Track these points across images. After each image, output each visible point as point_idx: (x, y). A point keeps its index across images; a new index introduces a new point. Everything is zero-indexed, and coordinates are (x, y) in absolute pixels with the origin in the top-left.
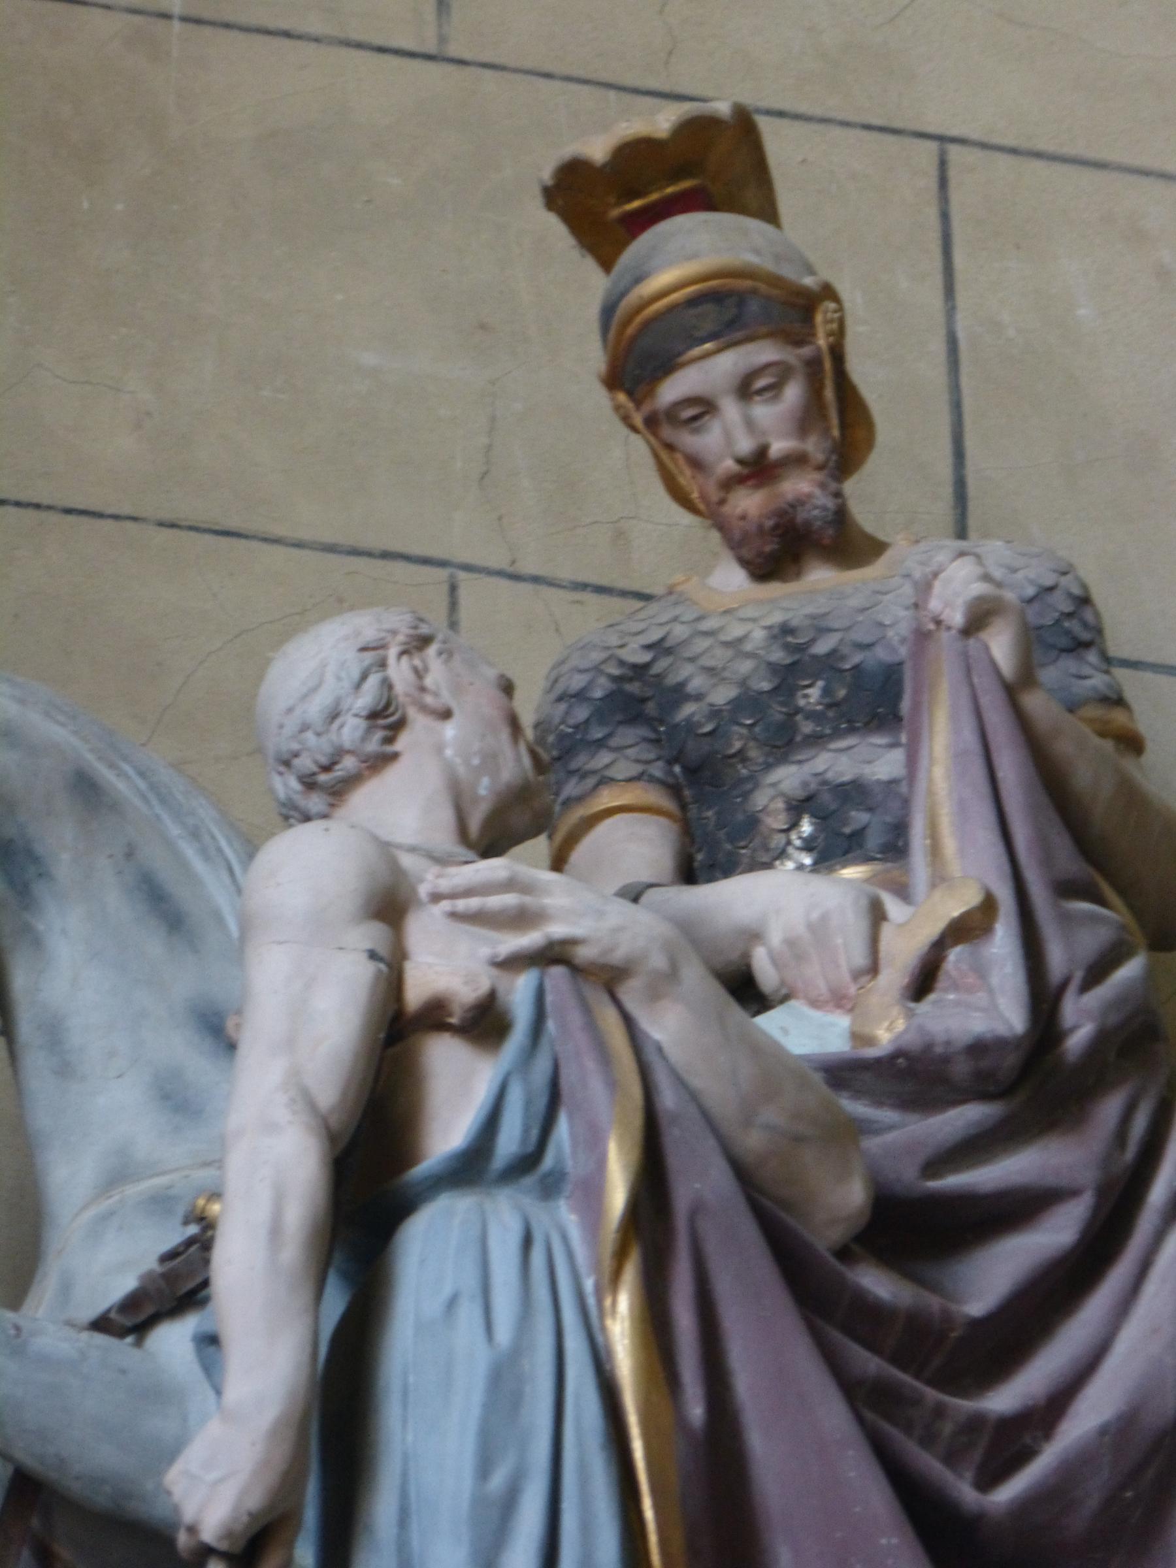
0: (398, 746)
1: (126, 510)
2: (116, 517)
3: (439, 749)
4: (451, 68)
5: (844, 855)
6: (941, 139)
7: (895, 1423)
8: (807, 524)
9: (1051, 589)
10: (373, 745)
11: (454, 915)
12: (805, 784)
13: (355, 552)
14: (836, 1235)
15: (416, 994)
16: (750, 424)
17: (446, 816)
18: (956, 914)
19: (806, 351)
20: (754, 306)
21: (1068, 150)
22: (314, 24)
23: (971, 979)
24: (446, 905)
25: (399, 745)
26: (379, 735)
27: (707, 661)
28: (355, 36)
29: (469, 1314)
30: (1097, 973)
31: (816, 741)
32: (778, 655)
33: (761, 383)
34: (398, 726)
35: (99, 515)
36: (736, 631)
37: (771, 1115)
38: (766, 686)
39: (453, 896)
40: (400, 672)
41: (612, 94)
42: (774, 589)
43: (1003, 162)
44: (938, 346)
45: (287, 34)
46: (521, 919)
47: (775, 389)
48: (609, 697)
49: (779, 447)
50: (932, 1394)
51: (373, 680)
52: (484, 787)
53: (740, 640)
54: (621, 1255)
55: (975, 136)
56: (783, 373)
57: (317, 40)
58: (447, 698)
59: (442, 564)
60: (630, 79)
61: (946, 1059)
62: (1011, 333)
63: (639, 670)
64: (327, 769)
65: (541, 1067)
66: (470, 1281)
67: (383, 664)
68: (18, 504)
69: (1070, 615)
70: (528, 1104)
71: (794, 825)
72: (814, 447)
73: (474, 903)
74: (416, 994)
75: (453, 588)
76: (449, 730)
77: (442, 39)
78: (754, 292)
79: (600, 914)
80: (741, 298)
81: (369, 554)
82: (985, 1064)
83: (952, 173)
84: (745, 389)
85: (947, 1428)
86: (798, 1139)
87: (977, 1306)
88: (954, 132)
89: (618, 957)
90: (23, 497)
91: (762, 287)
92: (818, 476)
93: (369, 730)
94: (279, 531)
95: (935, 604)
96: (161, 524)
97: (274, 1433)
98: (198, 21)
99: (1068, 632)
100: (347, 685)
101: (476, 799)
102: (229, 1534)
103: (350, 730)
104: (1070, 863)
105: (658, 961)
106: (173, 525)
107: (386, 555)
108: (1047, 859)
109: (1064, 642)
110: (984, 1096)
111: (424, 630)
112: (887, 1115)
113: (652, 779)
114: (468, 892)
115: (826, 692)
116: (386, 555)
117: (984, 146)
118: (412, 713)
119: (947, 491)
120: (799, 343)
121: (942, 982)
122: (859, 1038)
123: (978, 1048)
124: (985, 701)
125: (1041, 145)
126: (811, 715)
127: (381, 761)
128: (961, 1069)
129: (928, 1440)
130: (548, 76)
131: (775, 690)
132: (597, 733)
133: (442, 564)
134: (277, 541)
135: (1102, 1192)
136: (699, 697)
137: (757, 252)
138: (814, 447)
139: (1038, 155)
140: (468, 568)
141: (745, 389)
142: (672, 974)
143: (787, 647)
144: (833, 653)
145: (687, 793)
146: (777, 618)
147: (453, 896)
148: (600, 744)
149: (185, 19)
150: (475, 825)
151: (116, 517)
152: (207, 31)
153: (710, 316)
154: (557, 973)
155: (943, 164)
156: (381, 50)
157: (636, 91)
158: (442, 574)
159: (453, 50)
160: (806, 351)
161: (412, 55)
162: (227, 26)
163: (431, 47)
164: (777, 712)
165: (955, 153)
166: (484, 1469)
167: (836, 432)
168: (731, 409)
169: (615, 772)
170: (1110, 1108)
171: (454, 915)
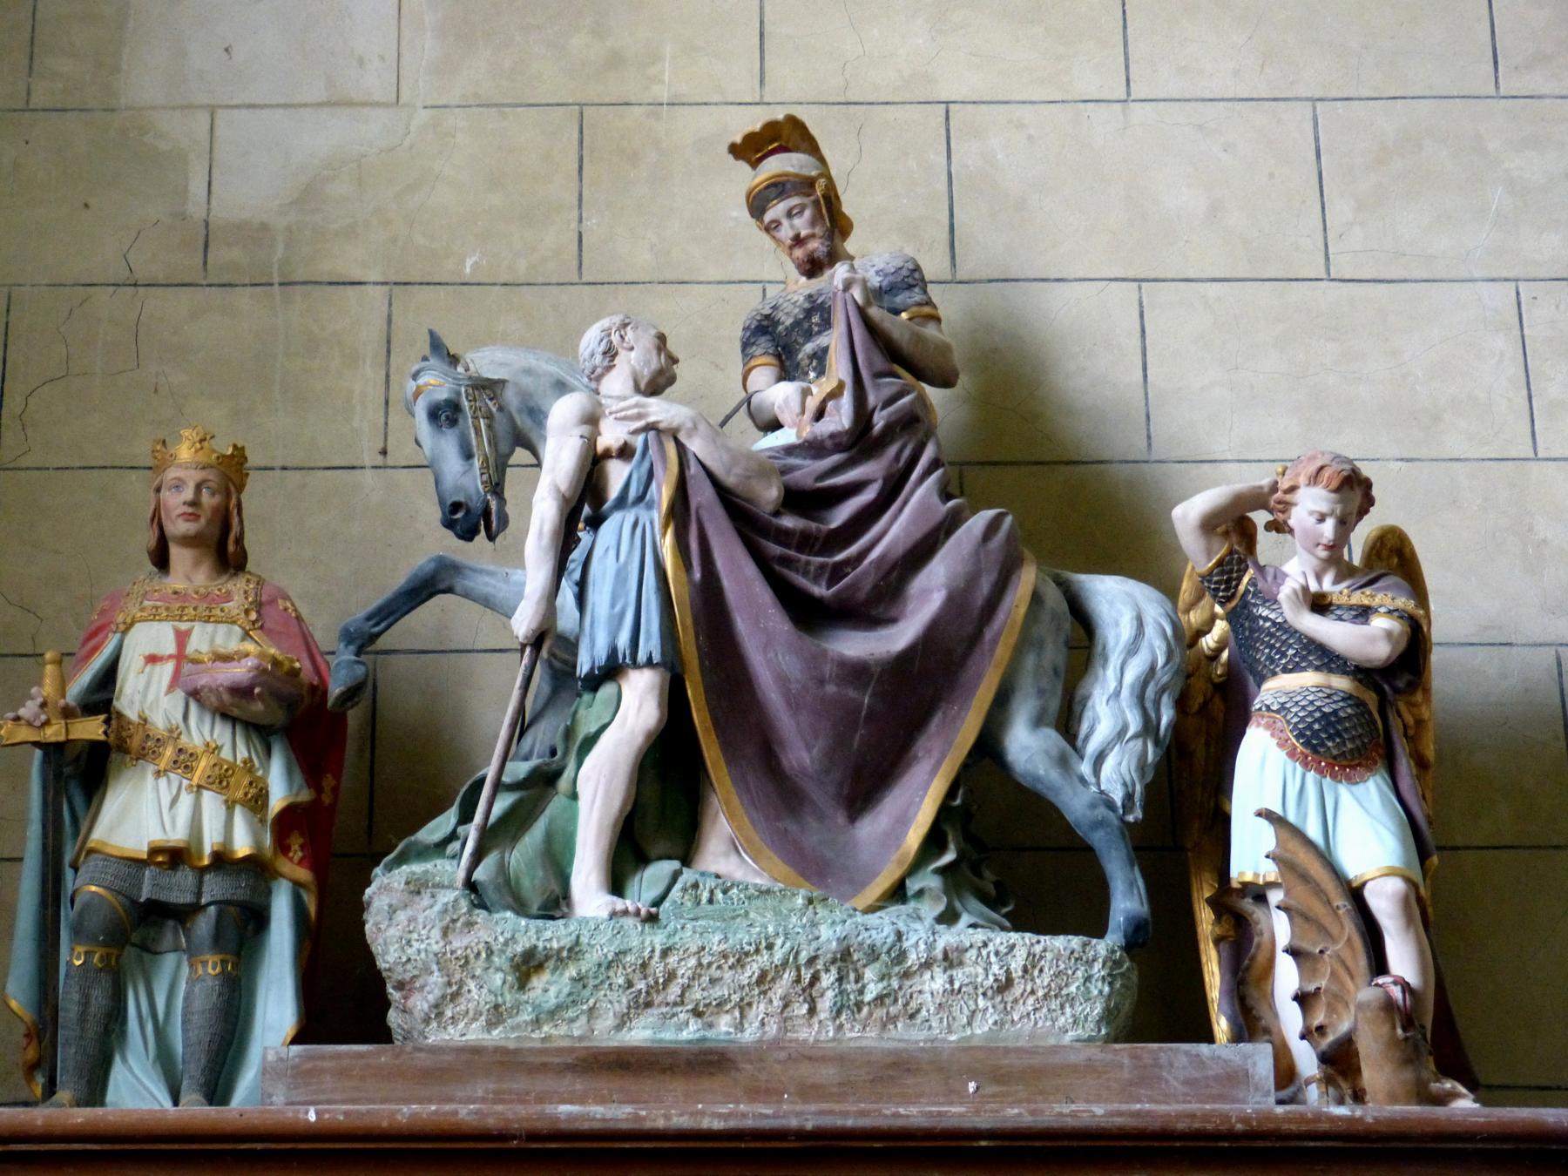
0: (616, 362)
1: (647, 280)
2: (643, 283)
3: (629, 362)
4: (765, 107)
5: (413, 416)
6: (947, 103)
7: (790, 569)
8: (819, 258)
9: (901, 268)
10: (606, 363)
11: (616, 419)
12: (813, 349)
13: (729, 282)
14: (770, 508)
15: (600, 447)
16: (792, 226)
17: (631, 384)
18: (829, 390)
19: (812, 198)
20: (789, 186)
21: (996, 99)
22: (715, 99)
23: (834, 412)
24: (614, 416)
25: (616, 362)
26: (608, 359)
27: (786, 311)
28: (730, 100)
29: (612, 553)
30: (888, 403)
31: (819, 333)
32: (807, 305)
33: (794, 212)
34: (614, 356)
35: (638, 283)
36: (796, 298)
37: (737, 470)
38: (801, 316)
39: (616, 412)
40: (615, 338)
41: (824, 106)
42: (814, 281)
43: (970, 107)
44: (944, 178)
45: (705, 104)
46: (639, 416)
47: (801, 213)
48: (757, 327)
49: (803, 233)
50: (804, 557)
51: (605, 341)
52: (646, 372)
53: (796, 302)
54: (666, 527)
55: (960, 100)
56: (802, 208)
57: (716, 104)
58: (632, 343)
59: (761, 282)
60: (831, 100)
61: (822, 441)
62: (972, 168)
63: (767, 317)
64: (593, 373)
65: (646, 465)
66: (613, 543)
67: (610, 335)
68: (609, 283)
69: (908, 277)
70: (639, 479)
71: (811, 363)
72: (818, 230)
73: (623, 414)
74: (600, 447)
75: (764, 290)
76: (633, 354)
77: (762, 96)
78: (788, 181)
79: (668, 411)
80: (783, 184)
81: (734, 282)
82: (837, 440)
83: (951, 114)
84: (789, 214)
85: (812, 568)
86: (749, 478)
87: (834, 525)
88: (952, 99)
89: (675, 425)
90: (610, 280)
91: (791, 178)
92: (820, 241)
93: (604, 359)
94: (702, 279)
95: (835, 283)
96: (660, 283)
97: (538, 603)
98: (673, 104)
99: (907, 283)
100: (597, 343)
101: (643, 376)
102: (526, 637)
103: (598, 359)
104: (880, 363)
105: (689, 425)
106: (663, 283)
107: (740, 282)
108: (870, 364)
109: (905, 286)
110: (840, 452)
111: (627, 321)
112: (808, 462)
113: (769, 354)
114: (622, 410)
115: (821, 316)
116: (740, 282)
117: (963, 102)
118: (620, 350)
119: (947, 229)
120: (809, 196)
121: (826, 414)
122: (798, 435)
123: (832, 436)
124: (850, 314)
125: (985, 99)
126: (817, 325)
127: (609, 368)
128: (829, 443)
129: (805, 574)
130: (800, 103)
131: (804, 318)
132: (752, 341)
133: (761, 282)
134: (701, 283)
135: (886, 480)
136: (783, 323)
137: (792, 166)
138: (818, 230)
139: (984, 103)
140: (770, 282)
141: (789, 214)
142: (695, 427)
143: (810, 302)
144: (822, 303)
145: (784, 357)
146: (807, 292)
147: (616, 412)
148: (753, 344)
149: (667, 104)
150: (643, 386)
151: (643, 283)
152: (676, 107)
153: (774, 191)
154: (652, 434)
155: (947, 112)
156: (740, 104)
157: (833, 104)
158: (760, 285)
159: (765, 100)
160: (812, 198)
161: (751, 104)
162: (684, 104)
163: (757, 100)
164: (806, 325)
165: (952, 107)
166: (613, 606)
167: (828, 224)
168: (785, 222)
169: (756, 354)
170: (892, 450)
171: (616, 419)
